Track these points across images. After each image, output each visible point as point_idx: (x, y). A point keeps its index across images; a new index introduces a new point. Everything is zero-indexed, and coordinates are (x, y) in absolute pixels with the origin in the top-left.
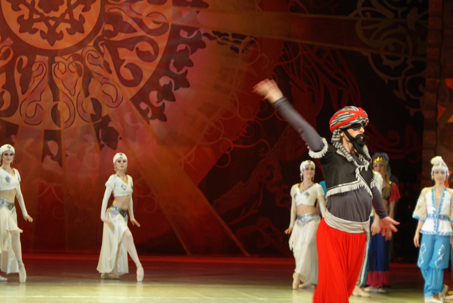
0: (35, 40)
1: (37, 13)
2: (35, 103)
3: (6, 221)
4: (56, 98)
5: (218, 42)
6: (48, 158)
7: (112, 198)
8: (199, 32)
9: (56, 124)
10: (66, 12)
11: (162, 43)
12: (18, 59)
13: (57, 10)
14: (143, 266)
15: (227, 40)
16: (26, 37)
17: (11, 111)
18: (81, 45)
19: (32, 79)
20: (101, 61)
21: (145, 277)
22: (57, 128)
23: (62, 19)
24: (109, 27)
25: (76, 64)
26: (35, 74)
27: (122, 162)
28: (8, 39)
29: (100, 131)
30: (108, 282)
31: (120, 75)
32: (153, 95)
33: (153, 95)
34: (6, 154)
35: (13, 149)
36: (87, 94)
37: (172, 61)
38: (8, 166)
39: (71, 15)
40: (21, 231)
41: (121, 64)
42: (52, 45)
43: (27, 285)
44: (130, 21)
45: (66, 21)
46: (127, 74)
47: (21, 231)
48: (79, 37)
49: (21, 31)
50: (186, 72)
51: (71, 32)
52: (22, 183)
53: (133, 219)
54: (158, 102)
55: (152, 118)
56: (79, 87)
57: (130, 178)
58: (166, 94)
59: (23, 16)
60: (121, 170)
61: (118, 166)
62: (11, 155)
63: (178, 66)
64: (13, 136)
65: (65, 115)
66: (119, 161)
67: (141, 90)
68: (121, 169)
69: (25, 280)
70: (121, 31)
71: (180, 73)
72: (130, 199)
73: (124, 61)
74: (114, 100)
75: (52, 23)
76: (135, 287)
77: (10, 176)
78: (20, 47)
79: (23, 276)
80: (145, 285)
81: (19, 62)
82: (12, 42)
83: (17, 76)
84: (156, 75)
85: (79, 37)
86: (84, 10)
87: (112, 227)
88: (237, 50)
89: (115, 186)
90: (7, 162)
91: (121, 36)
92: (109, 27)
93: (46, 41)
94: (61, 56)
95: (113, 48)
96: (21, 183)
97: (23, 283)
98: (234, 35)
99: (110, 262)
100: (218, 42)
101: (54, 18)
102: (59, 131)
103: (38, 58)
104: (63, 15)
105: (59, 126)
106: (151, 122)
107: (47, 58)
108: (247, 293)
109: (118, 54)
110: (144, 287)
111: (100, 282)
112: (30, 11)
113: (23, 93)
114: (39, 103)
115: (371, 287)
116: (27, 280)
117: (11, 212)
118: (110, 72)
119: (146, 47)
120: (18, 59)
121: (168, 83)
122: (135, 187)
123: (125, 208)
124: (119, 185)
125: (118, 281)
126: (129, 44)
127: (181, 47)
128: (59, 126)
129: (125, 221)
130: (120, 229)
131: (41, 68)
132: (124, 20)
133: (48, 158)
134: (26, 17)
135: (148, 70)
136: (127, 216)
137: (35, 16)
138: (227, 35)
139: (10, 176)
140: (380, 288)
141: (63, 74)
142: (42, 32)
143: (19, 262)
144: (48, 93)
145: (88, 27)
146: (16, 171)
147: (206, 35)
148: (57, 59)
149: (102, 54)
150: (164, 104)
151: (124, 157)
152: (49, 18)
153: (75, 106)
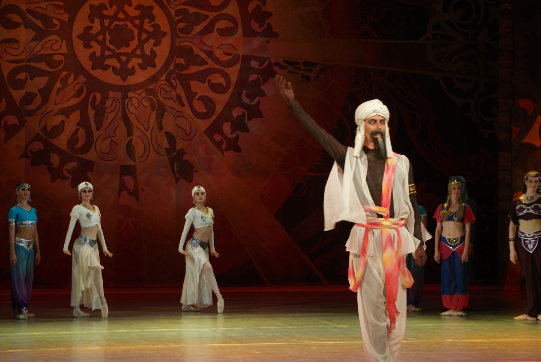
0: (109, 77)
1: (109, 49)
2: (110, 139)
3: (87, 257)
4: (130, 133)
5: (289, 71)
6: (124, 193)
7: (192, 229)
8: (270, 62)
9: (130, 157)
10: (137, 47)
11: (234, 73)
12: (92, 96)
13: (128, 46)
14: (223, 297)
15: (299, 68)
16: (98, 73)
17: (86, 149)
18: (154, 79)
19: (106, 115)
20: (173, 94)
21: (225, 308)
22: (132, 163)
23: (133, 54)
24: (182, 61)
25: (149, 99)
26: (108, 110)
27: (200, 195)
28: (81, 76)
29: (176, 164)
30: (189, 315)
31: (192, 105)
32: (227, 128)
33: (227, 128)
34: (85, 192)
35: (90, 186)
36: (161, 128)
37: (245, 92)
38: (88, 203)
39: (143, 50)
40: (103, 268)
41: (194, 97)
42: (124, 81)
43: (109, 320)
44: (203, 55)
45: (138, 56)
46: (201, 108)
47: (103, 268)
48: (151, 71)
49: (93, 68)
50: (259, 101)
51: (143, 67)
52: (102, 218)
53: (213, 251)
54: (232, 133)
55: (227, 150)
56: (153, 120)
57: (211, 210)
58: (239, 126)
59: (95, 53)
60: (200, 203)
61: (197, 198)
62: (90, 191)
63: (251, 97)
64: (89, 173)
65: (139, 150)
66: (197, 194)
67: (215, 121)
68: (199, 201)
69: (107, 316)
70: (194, 65)
71: (253, 103)
72: (211, 232)
73: (196, 93)
74: (188, 133)
75: (100, 38)
76: (216, 318)
77: (91, 212)
78: (94, 84)
79: (105, 312)
80: (226, 316)
81: (93, 98)
82: (85, 79)
83: (91, 113)
84: (229, 107)
85: (151, 71)
86: (155, 45)
87: (193, 260)
88: (308, 79)
89: (194, 219)
90: (86, 198)
91: (194, 69)
92: (182, 61)
93: (118, 78)
94: (133, 91)
95: (185, 81)
96: (101, 218)
97: (105, 318)
98: (305, 64)
99: (193, 293)
100: (289, 71)
101: (125, 54)
102: (135, 166)
103: (111, 94)
104: (134, 50)
105: (134, 161)
106: (225, 153)
107: (120, 94)
108: (327, 321)
109: (190, 87)
110: (225, 318)
111: (181, 315)
112: (101, 48)
113: (98, 129)
114: (113, 138)
115: (451, 310)
116: (110, 315)
117: (93, 249)
118: (183, 105)
119: (218, 79)
120: (92, 96)
121: (241, 114)
122: (215, 218)
123: (205, 240)
124: (200, 217)
125: (199, 313)
126: (202, 77)
127: (253, 77)
128: (134, 161)
129: (206, 253)
130: (200, 261)
131: (114, 104)
132: (195, 52)
133: (124, 193)
134: (98, 54)
135: (221, 100)
136: (207, 249)
137: (107, 53)
138: (298, 64)
139: (91, 212)
140: (460, 311)
141: (136, 109)
142: (113, 68)
143: (101, 298)
144: (122, 130)
145: (160, 62)
146: (96, 208)
147: (277, 64)
148: (130, 94)
149: (175, 88)
150: (237, 134)
151: (202, 189)
152: (121, 54)
153: (150, 140)
